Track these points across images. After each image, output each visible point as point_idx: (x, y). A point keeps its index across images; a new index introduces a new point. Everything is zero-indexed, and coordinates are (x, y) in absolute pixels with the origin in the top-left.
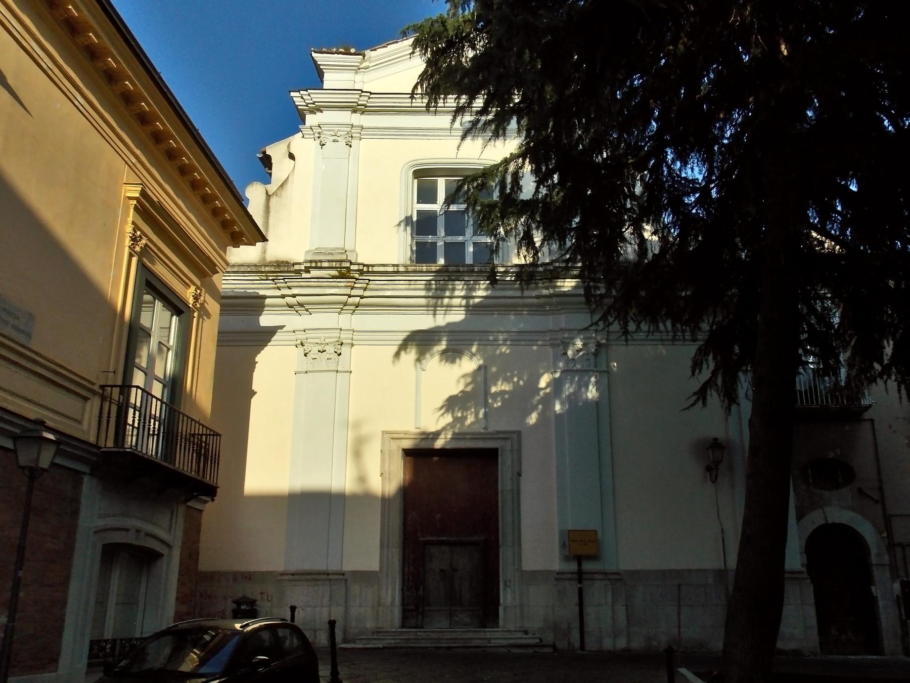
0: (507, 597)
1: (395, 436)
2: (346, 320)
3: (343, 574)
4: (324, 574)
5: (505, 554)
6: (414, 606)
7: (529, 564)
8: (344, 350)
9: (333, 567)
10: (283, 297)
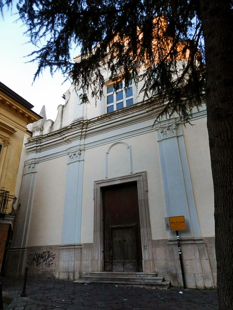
0: (146, 255)
1: (98, 182)
2: (82, 142)
3: (81, 245)
4: (73, 246)
5: (143, 231)
6: (108, 261)
7: (155, 237)
8: (82, 152)
9: (77, 242)
10: (63, 139)
